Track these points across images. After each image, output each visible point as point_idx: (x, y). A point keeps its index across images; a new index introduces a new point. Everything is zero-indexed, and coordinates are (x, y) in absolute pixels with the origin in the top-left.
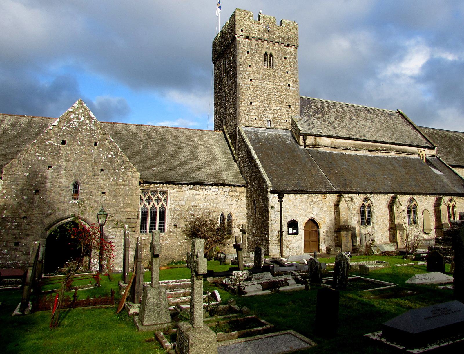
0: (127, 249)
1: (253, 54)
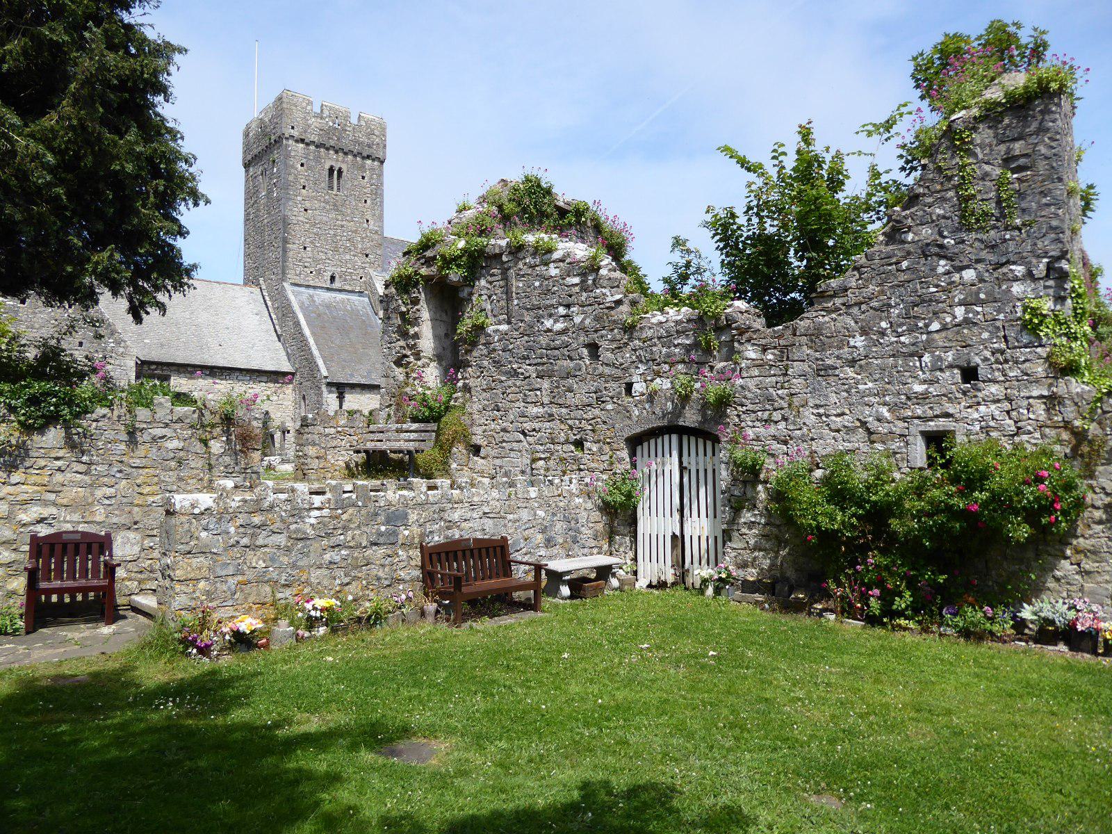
0: (182, 370)
1: (309, 168)
